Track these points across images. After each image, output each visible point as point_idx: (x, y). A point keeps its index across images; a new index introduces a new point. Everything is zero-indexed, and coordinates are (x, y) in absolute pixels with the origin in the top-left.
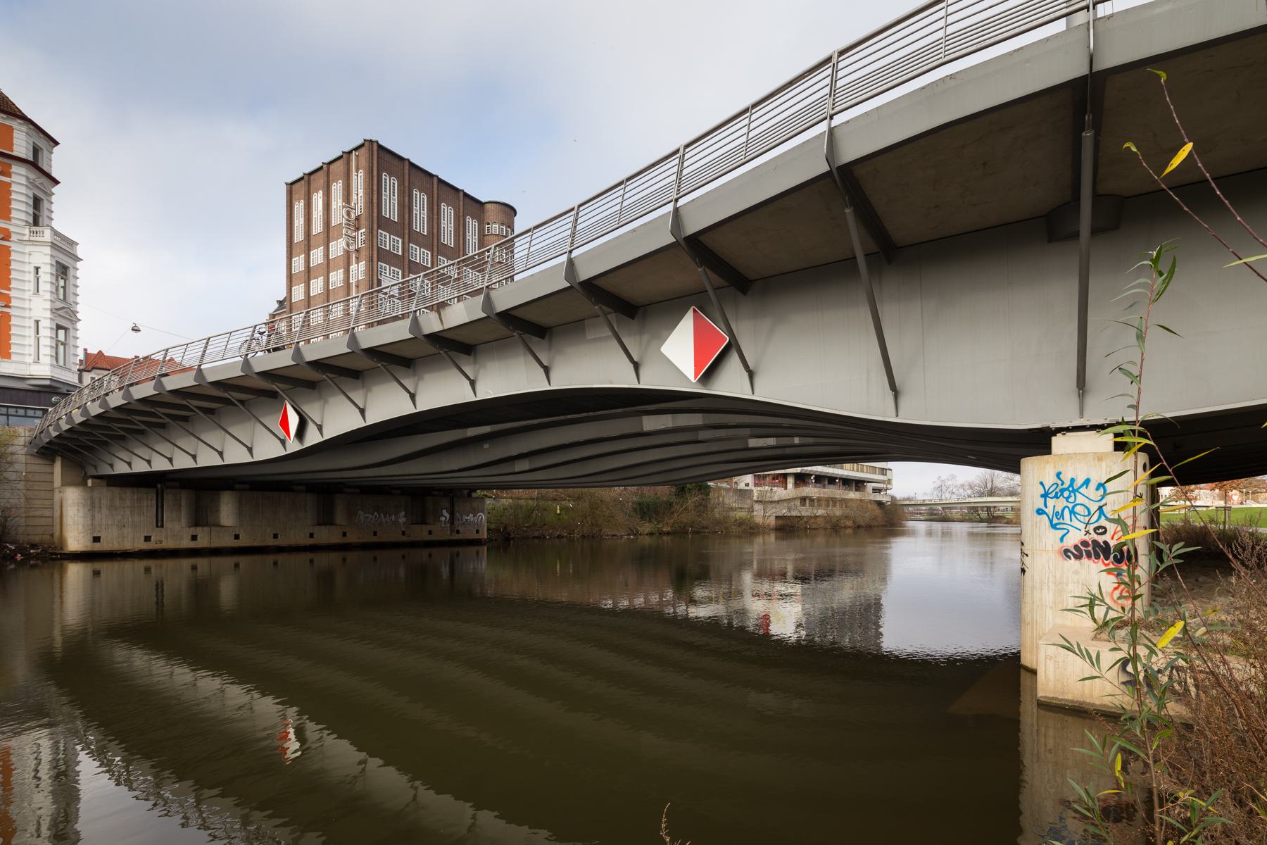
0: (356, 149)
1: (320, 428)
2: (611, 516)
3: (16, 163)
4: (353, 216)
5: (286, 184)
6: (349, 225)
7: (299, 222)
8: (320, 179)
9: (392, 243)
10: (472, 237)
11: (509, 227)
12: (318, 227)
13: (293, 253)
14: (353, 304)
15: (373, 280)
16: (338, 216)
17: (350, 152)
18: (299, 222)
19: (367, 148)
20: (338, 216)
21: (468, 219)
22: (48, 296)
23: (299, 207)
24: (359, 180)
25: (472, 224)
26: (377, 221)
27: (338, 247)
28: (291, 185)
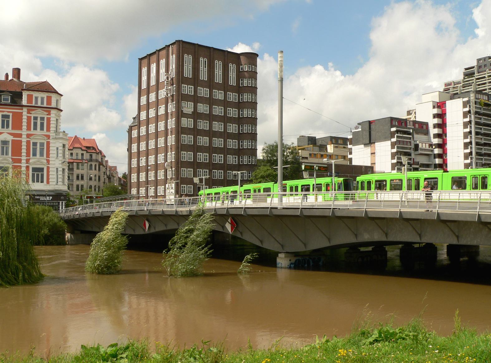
0: (172, 44)
1: (155, 228)
2: (138, 341)
3: (52, 109)
4: (170, 79)
5: (139, 59)
6: (168, 84)
7: (144, 78)
8: (154, 58)
9: (188, 89)
10: (232, 75)
11: (254, 65)
12: (153, 82)
13: (141, 94)
14: (170, 106)
15: (179, 108)
16: (163, 78)
17: (170, 45)
18: (144, 78)
19: (177, 44)
20: (163, 78)
21: (230, 65)
22: (61, 159)
23: (145, 70)
24: (173, 59)
25: (232, 67)
26: (180, 79)
27: (162, 93)
28: (141, 59)
